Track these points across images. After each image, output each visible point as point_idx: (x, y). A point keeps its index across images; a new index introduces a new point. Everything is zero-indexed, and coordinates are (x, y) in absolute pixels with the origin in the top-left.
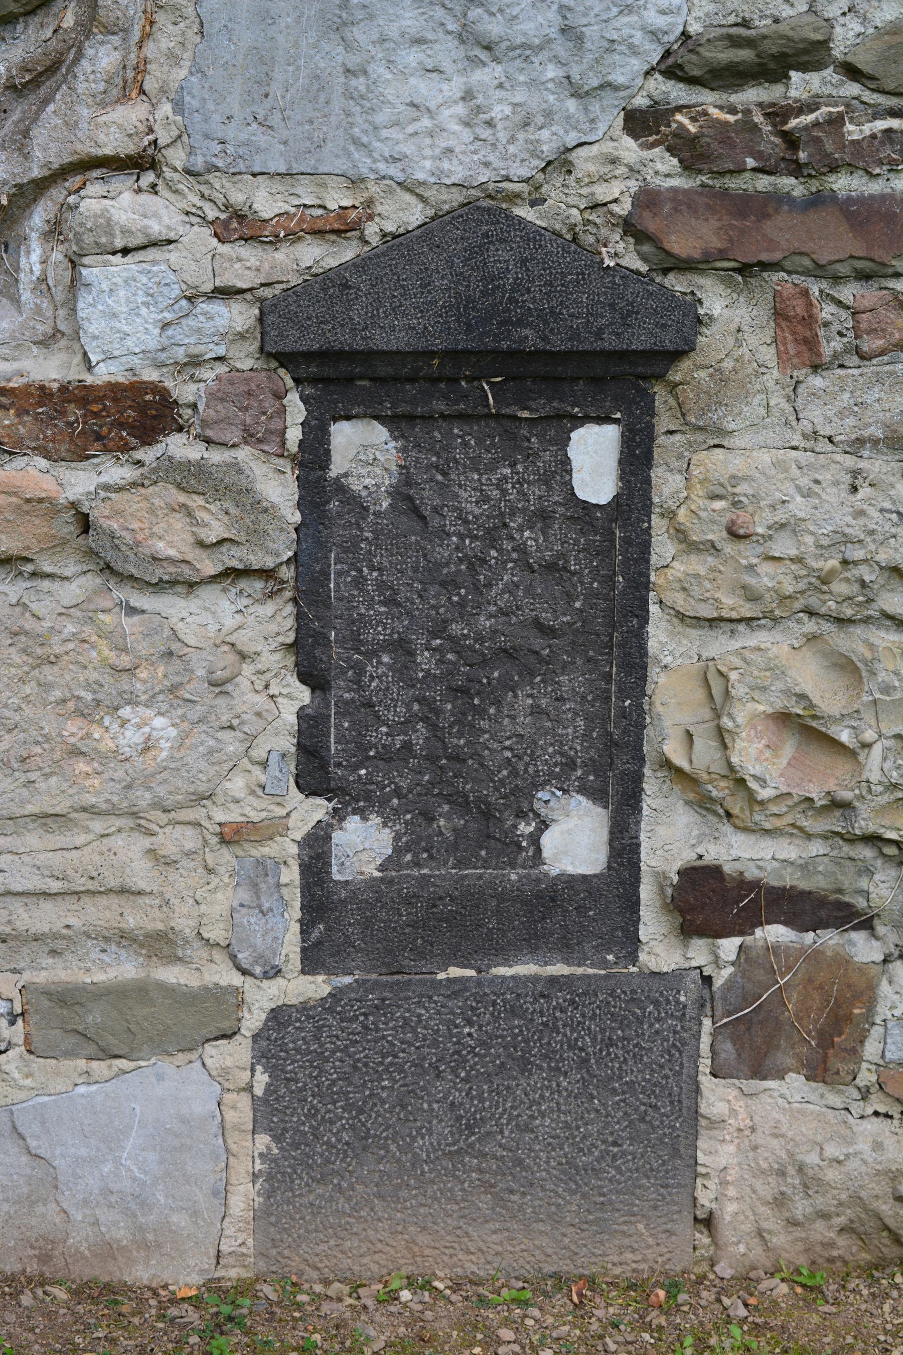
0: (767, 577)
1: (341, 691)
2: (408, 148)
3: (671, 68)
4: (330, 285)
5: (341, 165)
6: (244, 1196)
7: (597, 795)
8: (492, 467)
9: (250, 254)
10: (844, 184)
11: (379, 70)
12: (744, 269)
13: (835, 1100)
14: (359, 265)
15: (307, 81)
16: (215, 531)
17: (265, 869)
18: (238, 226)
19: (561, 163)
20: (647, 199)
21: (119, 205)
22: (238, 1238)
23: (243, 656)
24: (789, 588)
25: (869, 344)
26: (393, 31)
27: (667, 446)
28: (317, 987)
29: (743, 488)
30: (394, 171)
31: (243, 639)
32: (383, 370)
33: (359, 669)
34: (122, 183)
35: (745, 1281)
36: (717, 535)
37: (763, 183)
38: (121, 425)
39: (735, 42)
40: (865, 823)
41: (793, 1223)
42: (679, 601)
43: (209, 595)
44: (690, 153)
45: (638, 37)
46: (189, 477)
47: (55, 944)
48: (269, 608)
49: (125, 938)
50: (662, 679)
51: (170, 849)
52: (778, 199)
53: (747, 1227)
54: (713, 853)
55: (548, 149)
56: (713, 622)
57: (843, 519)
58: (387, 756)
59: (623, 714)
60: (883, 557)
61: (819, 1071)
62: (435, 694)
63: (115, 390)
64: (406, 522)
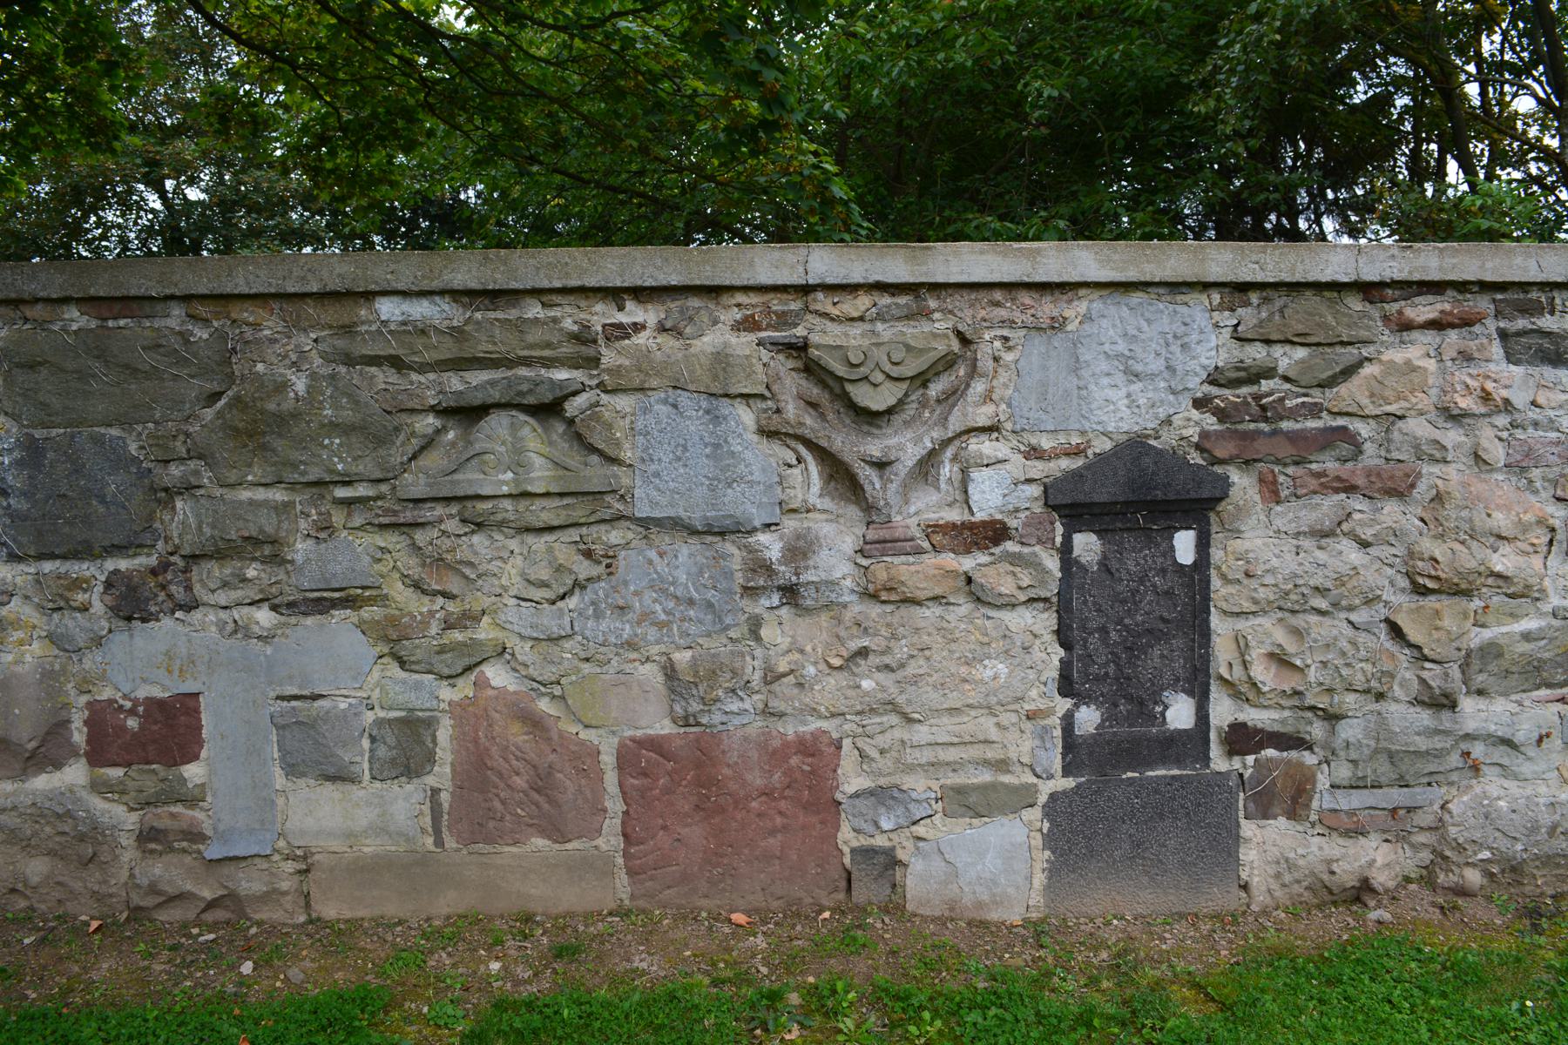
0: (1262, 594)
1: (1078, 651)
2: (1105, 418)
3: (1212, 381)
4: (1075, 476)
5: (1077, 426)
6: (1039, 879)
7: (1190, 693)
8: (1141, 551)
9: (1039, 464)
10: (1286, 425)
11: (1092, 387)
12: (1247, 462)
13: (1301, 829)
14: (1087, 467)
15: (1533, 520)
16: (1026, 582)
17: (1046, 729)
18: (1034, 453)
19: (1168, 422)
20: (1204, 435)
21: (984, 447)
22: (1036, 899)
23: (1036, 636)
24: (1272, 598)
25: (1300, 492)
26: (1098, 371)
27: (1217, 538)
28: (1070, 783)
29: (1251, 555)
30: (1099, 428)
31: (1035, 629)
32: (1097, 511)
33: (1085, 641)
34: (984, 437)
35: (1265, 912)
36: (1240, 576)
37: (1252, 426)
38: (985, 538)
39: (1238, 369)
40: (1310, 701)
41: (1284, 885)
42: (1224, 606)
43: (1021, 609)
44: (1222, 415)
45: (1198, 369)
46: (1015, 559)
47: (955, 767)
48: (1046, 615)
49: (986, 763)
50: (1218, 640)
51: (1005, 723)
52: (1258, 432)
53: (1264, 888)
54: (1242, 717)
55: (1162, 416)
56: (1238, 614)
57: (1294, 567)
58: (1097, 679)
59: (1201, 656)
60: (1311, 583)
61: (1292, 815)
62: (1118, 650)
63: (984, 524)
64: (1104, 576)
